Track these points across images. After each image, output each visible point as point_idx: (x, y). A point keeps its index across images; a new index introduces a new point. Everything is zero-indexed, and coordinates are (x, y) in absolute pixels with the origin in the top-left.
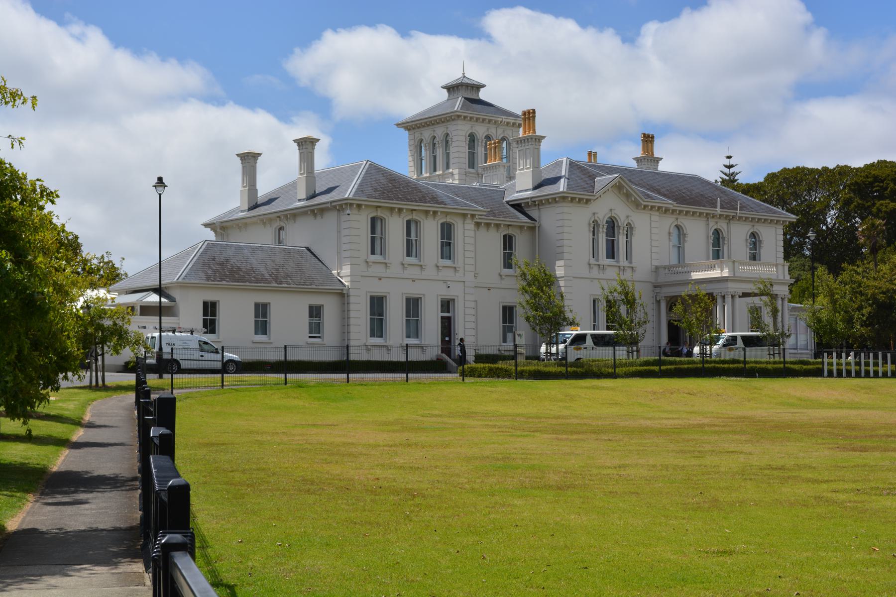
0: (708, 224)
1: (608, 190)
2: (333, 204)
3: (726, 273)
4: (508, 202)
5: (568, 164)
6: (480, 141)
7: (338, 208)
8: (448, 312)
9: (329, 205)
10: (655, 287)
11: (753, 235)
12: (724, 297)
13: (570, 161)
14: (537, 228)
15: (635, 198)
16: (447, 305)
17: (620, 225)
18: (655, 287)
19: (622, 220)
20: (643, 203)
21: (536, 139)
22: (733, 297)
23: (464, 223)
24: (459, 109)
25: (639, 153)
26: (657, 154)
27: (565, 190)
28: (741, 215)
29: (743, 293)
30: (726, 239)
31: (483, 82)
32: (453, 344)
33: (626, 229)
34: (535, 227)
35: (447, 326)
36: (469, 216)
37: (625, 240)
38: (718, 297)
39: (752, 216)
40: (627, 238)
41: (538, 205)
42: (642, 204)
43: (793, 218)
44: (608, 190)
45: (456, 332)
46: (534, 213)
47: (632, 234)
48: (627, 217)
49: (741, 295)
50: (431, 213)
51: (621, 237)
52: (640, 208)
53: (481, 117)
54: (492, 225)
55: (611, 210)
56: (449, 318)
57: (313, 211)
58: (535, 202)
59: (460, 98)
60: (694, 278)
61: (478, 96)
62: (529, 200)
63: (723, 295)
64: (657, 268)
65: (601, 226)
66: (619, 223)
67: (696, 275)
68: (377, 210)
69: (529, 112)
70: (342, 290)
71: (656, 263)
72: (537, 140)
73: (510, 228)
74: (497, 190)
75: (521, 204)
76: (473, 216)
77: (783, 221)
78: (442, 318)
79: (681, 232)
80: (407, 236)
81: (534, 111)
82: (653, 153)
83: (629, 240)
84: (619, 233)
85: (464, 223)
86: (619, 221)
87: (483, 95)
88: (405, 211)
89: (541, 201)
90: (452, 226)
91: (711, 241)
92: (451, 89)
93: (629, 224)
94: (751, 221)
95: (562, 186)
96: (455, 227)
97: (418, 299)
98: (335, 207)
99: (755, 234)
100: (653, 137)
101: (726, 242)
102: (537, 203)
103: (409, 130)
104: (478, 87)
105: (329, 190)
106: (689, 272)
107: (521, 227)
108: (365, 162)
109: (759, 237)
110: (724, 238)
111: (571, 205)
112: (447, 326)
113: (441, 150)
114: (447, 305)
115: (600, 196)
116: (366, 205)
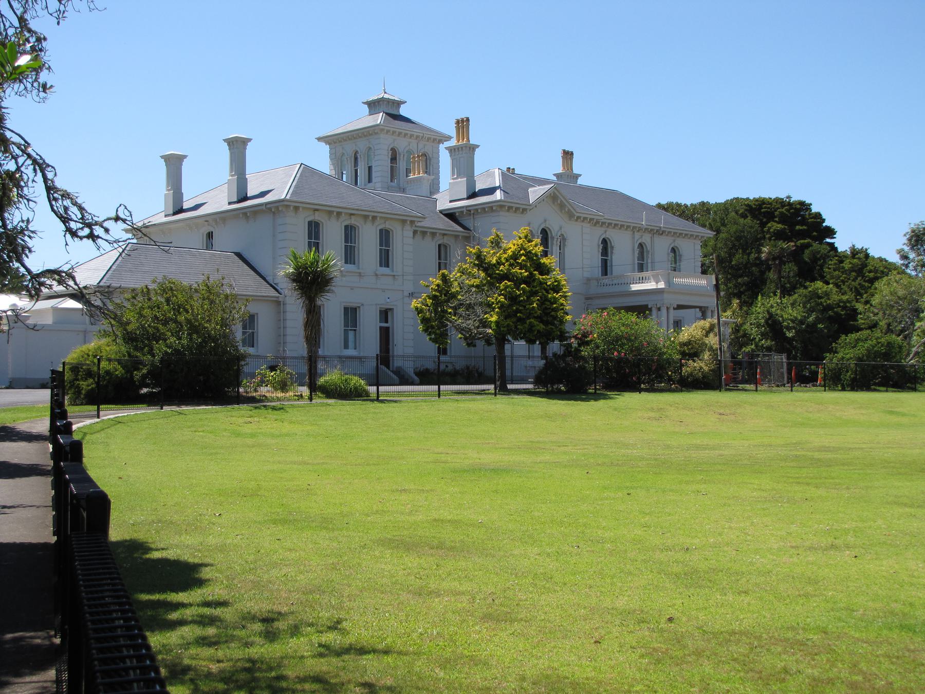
0: (633, 238)
1: (543, 200)
2: (268, 206)
3: (661, 285)
4: (441, 212)
5: (501, 175)
6: (402, 156)
7: (273, 210)
8: (387, 322)
9: (264, 207)
10: (587, 299)
11: (605, 242)
12: (659, 309)
13: (502, 172)
14: (472, 238)
15: (569, 210)
16: (385, 314)
17: (553, 235)
18: (587, 299)
19: (554, 230)
20: (575, 214)
21: (470, 148)
22: (668, 309)
23: (403, 230)
24: (382, 122)
25: (560, 170)
26: (576, 171)
27: (503, 198)
28: (664, 229)
29: (678, 305)
30: (650, 253)
31: (403, 99)
32: (391, 353)
33: (559, 240)
34: (470, 237)
35: (385, 335)
36: (408, 222)
37: (558, 251)
38: (653, 309)
39: (675, 231)
40: (560, 250)
41: (473, 214)
42: (575, 215)
43: (715, 233)
44: (543, 200)
45: (395, 343)
46: (469, 223)
47: (564, 245)
48: (561, 228)
49: (676, 307)
50: (370, 218)
51: (554, 248)
52: (573, 219)
53: (398, 130)
54: (428, 234)
55: (545, 221)
56: (388, 328)
57: (245, 214)
58: (470, 211)
59: (381, 114)
60: (633, 289)
61: (399, 111)
62: (465, 209)
63: (658, 306)
64: (589, 280)
65: (555, 239)
66: (553, 232)
67: (635, 287)
68: (314, 214)
69: (462, 120)
70: (278, 297)
71: (586, 275)
72: (472, 149)
73: (446, 237)
74: (429, 200)
75: (455, 213)
76: (412, 222)
77: (702, 237)
78: (381, 328)
79: (677, 254)
80: (345, 243)
81: (468, 120)
82: (572, 170)
83: (561, 251)
84: (552, 244)
85: (403, 230)
86: (552, 230)
87: (404, 111)
88: (343, 215)
89: (477, 210)
90: (321, 225)
91: (636, 255)
92: (373, 106)
93: (562, 235)
94: (673, 236)
95: (498, 195)
96: (360, 230)
97: (356, 308)
98: (270, 209)
99: (643, 245)
100: (572, 153)
101: (650, 256)
102: (472, 212)
103: (330, 144)
104: (398, 104)
105: (263, 194)
106: (629, 284)
107: (456, 237)
108: (299, 166)
109: (679, 252)
110: (648, 252)
111: (507, 214)
112: (385, 335)
113: (363, 163)
114: (385, 314)
115: (536, 206)
116: (304, 208)
